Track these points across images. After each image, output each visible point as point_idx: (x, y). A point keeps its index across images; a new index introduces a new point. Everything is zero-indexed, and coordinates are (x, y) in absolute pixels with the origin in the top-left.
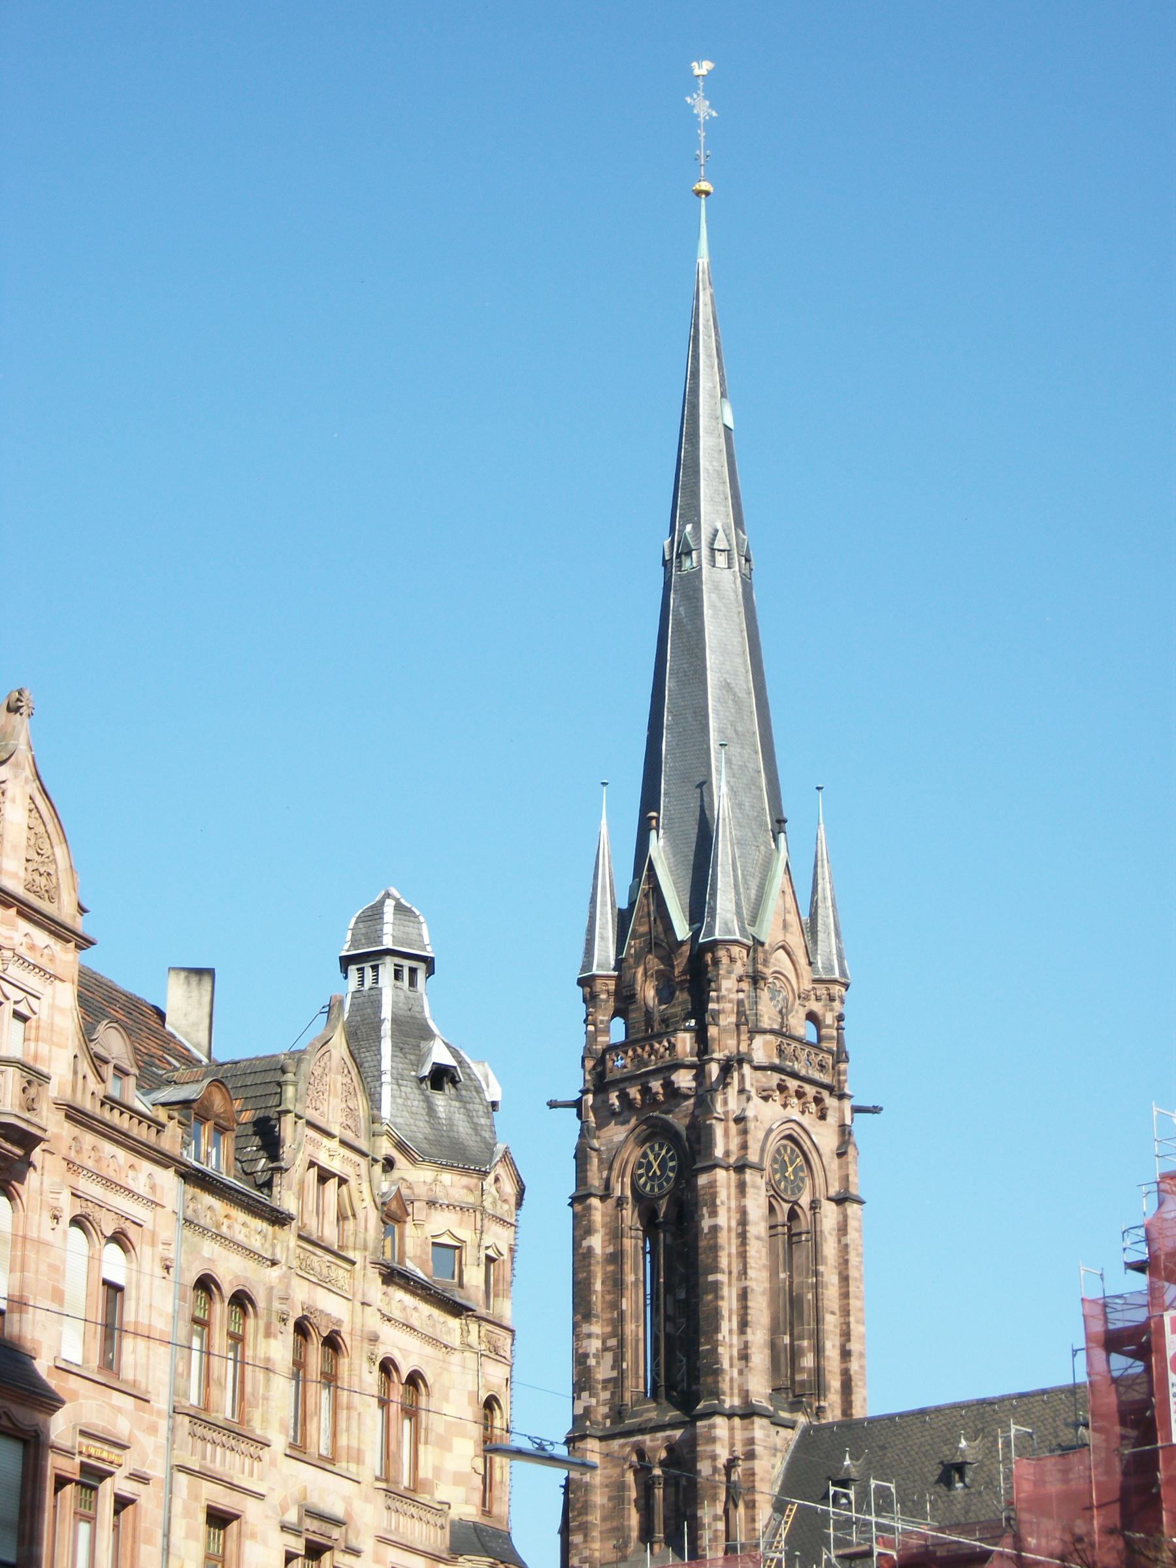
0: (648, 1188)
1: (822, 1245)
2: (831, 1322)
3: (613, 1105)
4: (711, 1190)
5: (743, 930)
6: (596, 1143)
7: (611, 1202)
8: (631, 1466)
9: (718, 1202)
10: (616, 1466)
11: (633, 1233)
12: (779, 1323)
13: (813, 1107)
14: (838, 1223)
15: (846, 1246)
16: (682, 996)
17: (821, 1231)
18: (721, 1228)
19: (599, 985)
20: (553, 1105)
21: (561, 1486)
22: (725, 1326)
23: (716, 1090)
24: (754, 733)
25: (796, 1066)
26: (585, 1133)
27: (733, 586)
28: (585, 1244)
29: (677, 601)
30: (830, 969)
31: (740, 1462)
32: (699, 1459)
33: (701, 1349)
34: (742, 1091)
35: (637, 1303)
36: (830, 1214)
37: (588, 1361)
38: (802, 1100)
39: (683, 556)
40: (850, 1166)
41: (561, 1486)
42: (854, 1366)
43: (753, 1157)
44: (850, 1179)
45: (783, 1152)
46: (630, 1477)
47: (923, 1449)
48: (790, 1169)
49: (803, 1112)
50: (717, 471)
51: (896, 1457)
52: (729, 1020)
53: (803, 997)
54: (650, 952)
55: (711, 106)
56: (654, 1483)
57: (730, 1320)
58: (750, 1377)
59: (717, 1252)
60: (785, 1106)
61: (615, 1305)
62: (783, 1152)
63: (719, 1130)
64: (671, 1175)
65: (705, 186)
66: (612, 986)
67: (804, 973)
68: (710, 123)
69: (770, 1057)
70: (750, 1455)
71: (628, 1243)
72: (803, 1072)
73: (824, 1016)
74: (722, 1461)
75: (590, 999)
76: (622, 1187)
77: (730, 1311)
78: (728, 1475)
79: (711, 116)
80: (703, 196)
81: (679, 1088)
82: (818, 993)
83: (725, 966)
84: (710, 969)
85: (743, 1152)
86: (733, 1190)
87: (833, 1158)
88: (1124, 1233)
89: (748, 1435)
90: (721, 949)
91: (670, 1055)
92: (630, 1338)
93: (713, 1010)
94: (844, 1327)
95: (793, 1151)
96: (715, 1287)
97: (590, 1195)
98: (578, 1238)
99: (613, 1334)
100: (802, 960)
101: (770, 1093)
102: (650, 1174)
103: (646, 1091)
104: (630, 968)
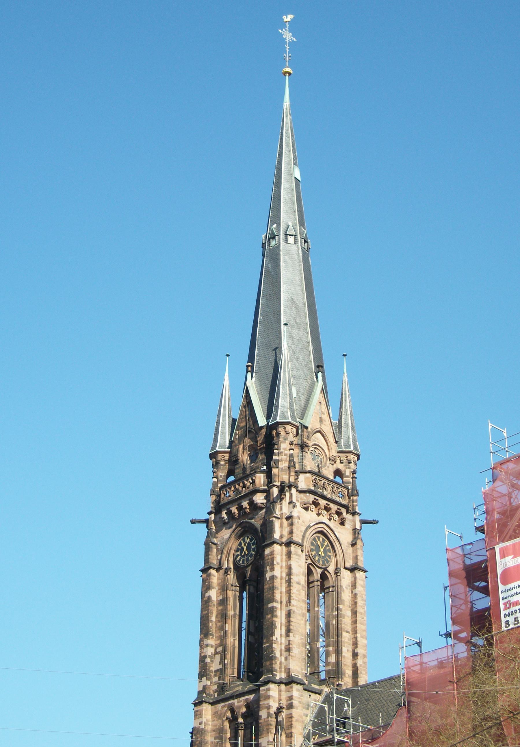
0: (241, 562)
1: (341, 593)
2: (346, 637)
3: (224, 518)
4: (272, 556)
5: (293, 417)
6: (215, 541)
7: (222, 572)
8: (227, 718)
9: (275, 562)
10: (219, 719)
11: (234, 588)
12: (314, 636)
13: (336, 517)
14: (351, 582)
15: (356, 594)
16: (262, 457)
17: (341, 586)
18: (277, 577)
19: (220, 457)
20: (193, 522)
21: (190, 733)
22: (277, 632)
23: (276, 502)
24: (306, 324)
25: (325, 493)
26: (210, 535)
27: (297, 252)
28: (207, 595)
29: (267, 261)
30: (348, 445)
31: (284, 710)
32: (261, 709)
33: (264, 646)
34: (291, 502)
35: (234, 626)
36: (346, 577)
37: (206, 660)
38: (329, 513)
39: (271, 240)
40: (358, 551)
41: (190, 733)
42: (360, 662)
43: (297, 537)
44: (358, 558)
45: (317, 540)
46: (227, 725)
47: (389, 698)
48: (322, 550)
49: (330, 519)
50: (291, 199)
51: (374, 704)
52: (284, 465)
53: (333, 460)
54: (246, 436)
55: (293, 36)
56: (238, 727)
57: (281, 629)
58: (291, 661)
59: (273, 590)
60: (319, 514)
61: (222, 628)
62: (317, 540)
63: (277, 524)
64: (253, 553)
65: (288, 70)
66: (227, 457)
67: (333, 447)
68: (291, 44)
69: (308, 486)
70: (290, 706)
71: (230, 594)
72: (329, 496)
73: (345, 471)
74: (273, 710)
75: (216, 465)
76: (228, 563)
77: (281, 624)
78: (277, 718)
79: (293, 40)
80: (287, 75)
81: (257, 503)
82: (342, 459)
83: (283, 436)
84: (275, 439)
85: (290, 536)
86: (284, 557)
87: (349, 547)
88: (474, 509)
89: (289, 694)
90: (281, 427)
91: (253, 486)
92: (230, 646)
93: (276, 460)
94: (354, 640)
95: (323, 540)
96: (272, 610)
97: (210, 568)
98: (203, 593)
99: (221, 645)
100: (331, 440)
101: (309, 505)
102: (243, 554)
103: (240, 508)
104: (236, 445)
